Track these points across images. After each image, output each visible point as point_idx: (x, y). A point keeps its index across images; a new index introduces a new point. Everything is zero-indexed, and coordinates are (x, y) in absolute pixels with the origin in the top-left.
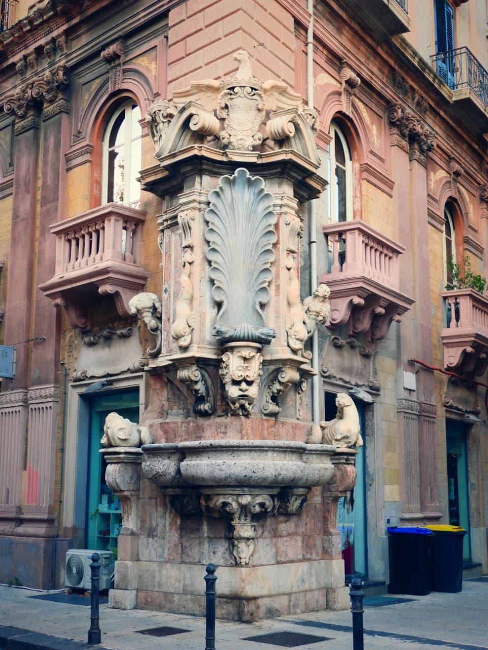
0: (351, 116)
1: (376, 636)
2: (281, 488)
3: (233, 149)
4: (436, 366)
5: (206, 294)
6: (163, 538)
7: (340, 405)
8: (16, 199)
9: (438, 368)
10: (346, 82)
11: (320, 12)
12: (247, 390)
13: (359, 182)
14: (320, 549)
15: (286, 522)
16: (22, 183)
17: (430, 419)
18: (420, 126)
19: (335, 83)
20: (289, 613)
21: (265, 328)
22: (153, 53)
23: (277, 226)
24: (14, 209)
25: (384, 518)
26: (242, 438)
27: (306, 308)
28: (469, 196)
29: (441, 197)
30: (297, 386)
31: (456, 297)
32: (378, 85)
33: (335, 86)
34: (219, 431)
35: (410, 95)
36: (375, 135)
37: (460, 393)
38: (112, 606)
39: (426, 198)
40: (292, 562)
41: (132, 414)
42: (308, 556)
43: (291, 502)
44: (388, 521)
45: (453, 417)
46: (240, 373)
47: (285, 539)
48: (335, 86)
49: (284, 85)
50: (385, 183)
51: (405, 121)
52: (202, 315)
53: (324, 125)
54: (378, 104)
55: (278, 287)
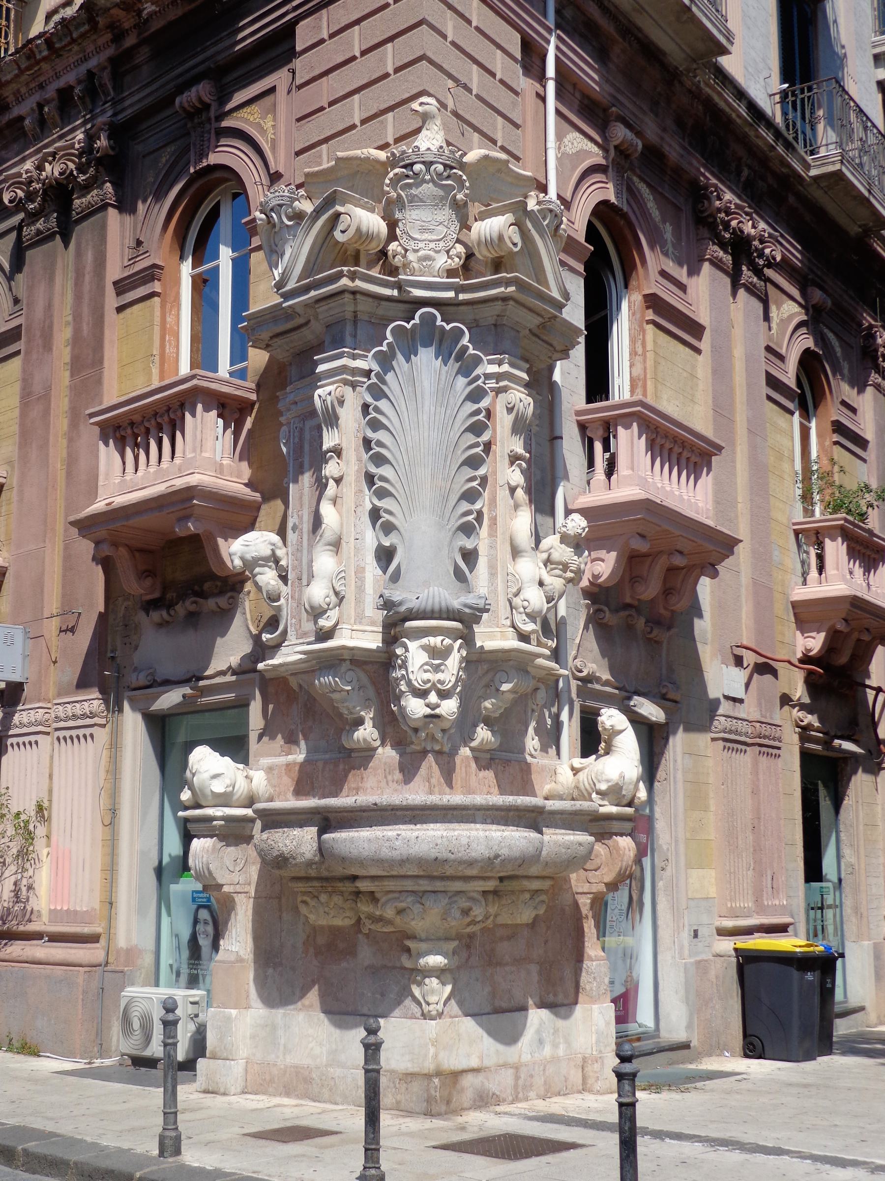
1: (667, 1140)
3: (412, 275)
5: (370, 539)
7: (605, 729)
8: (26, 362)
9: (786, 658)
10: (616, 147)
12: (438, 706)
17: (770, 750)
18: (751, 222)
19: (595, 149)
20: (516, 1100)
21: (471, 595)
22: (268, 101)
23: (489, 414)
24: (24, 380)
25: (686, 929)
26: (431, 793)
27: (545, 556)
28: (841, 346)
33: (596, 156)
34: (390, 778)
36: (669, 241)
38: (203, 1088)
39: (763, 352)
41: (235, 746)
46: (427, 676)
47: (507, 968)
48: (596, 156)
49: (503, 156)
51: (723, 215)
52: (360, 571)
53: (576, 226)
55: (494, 521)
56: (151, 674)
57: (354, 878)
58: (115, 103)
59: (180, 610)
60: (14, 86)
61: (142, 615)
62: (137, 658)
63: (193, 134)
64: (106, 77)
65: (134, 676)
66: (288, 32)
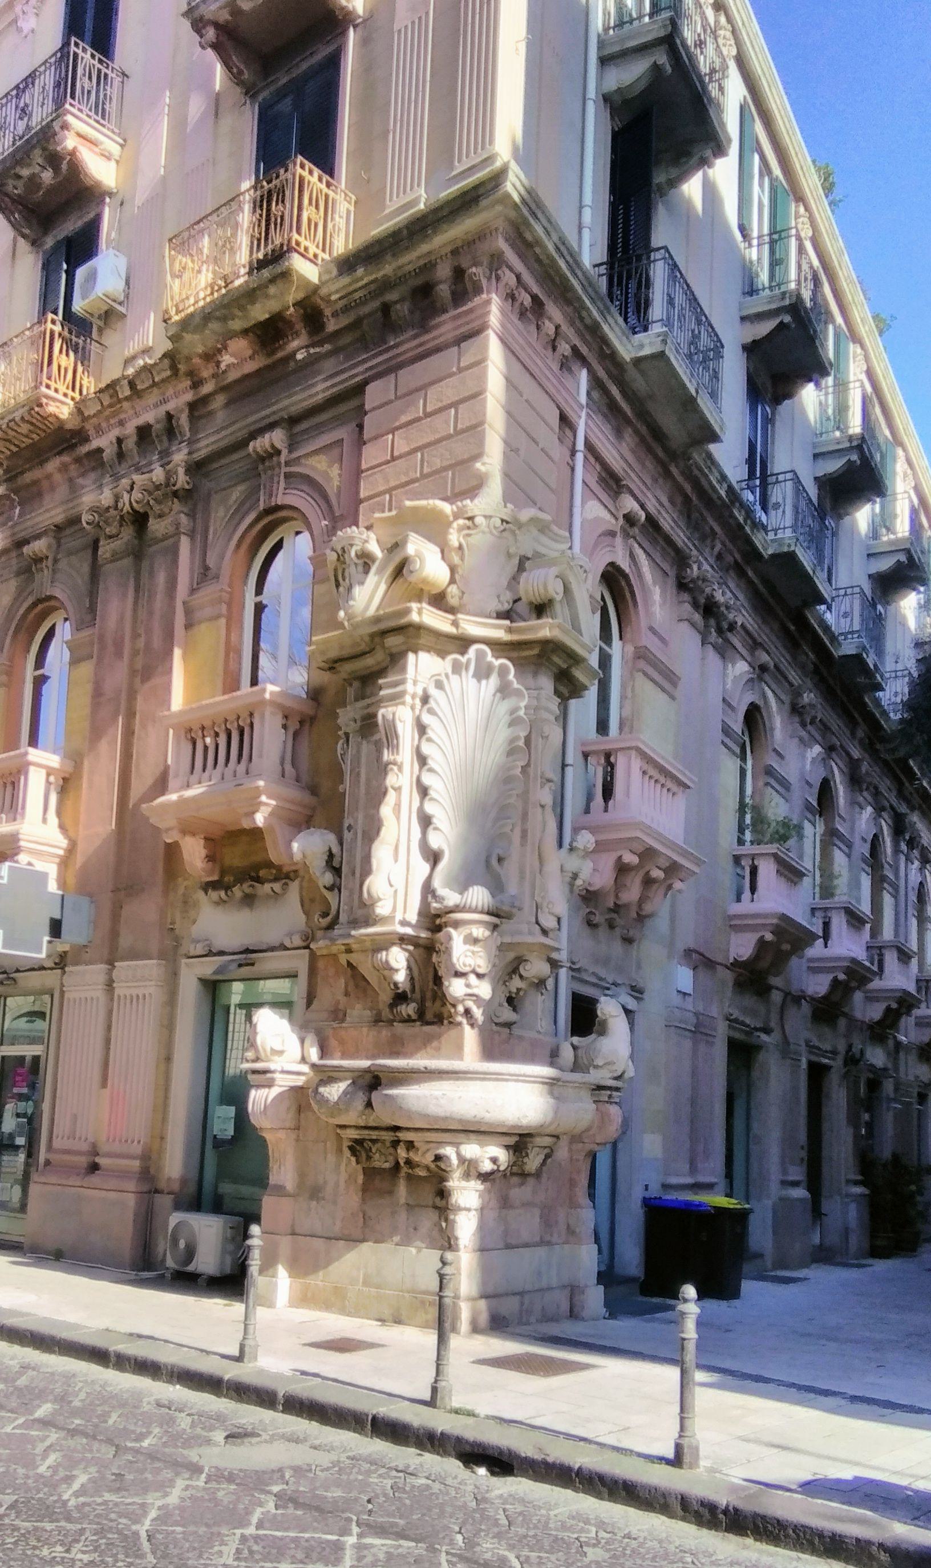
0: (627, 570)
2: (520, 1135)
4: (719, 958)
6: (335, 1203)
10: (624, 516)
11: (594, 402)
13: (631, 674)
14: (562, 1227)
15: (522, 1184)
16: (109, 642)
19: (608, 517)
20: (520, 1323)
22: (336, 451)
29: (740, 700)
30: (541, 983)
31: (753, 857)
32: (666, 522)
35: (708, 542)
37: (749, 1001)
39: (721, 703)
40: (526, 1245)
42: (547, 1238)
43: (531, 1156)
44: (647, 1187)
45: (737, 1035)
50: (667, 679)
54: (664, 554)
56: (209, 946)
57: (396, 1129)
58: (191, 442)
59: (237, 892)
60: (95, 420)
61: (201, 894)
62: (196, 930)
63: (263, 476)
64: (184, 420)
65: (192, 947)
66: (359, 390)
